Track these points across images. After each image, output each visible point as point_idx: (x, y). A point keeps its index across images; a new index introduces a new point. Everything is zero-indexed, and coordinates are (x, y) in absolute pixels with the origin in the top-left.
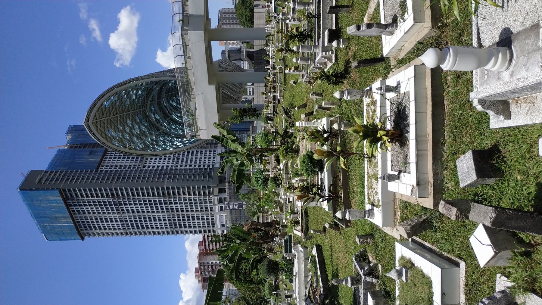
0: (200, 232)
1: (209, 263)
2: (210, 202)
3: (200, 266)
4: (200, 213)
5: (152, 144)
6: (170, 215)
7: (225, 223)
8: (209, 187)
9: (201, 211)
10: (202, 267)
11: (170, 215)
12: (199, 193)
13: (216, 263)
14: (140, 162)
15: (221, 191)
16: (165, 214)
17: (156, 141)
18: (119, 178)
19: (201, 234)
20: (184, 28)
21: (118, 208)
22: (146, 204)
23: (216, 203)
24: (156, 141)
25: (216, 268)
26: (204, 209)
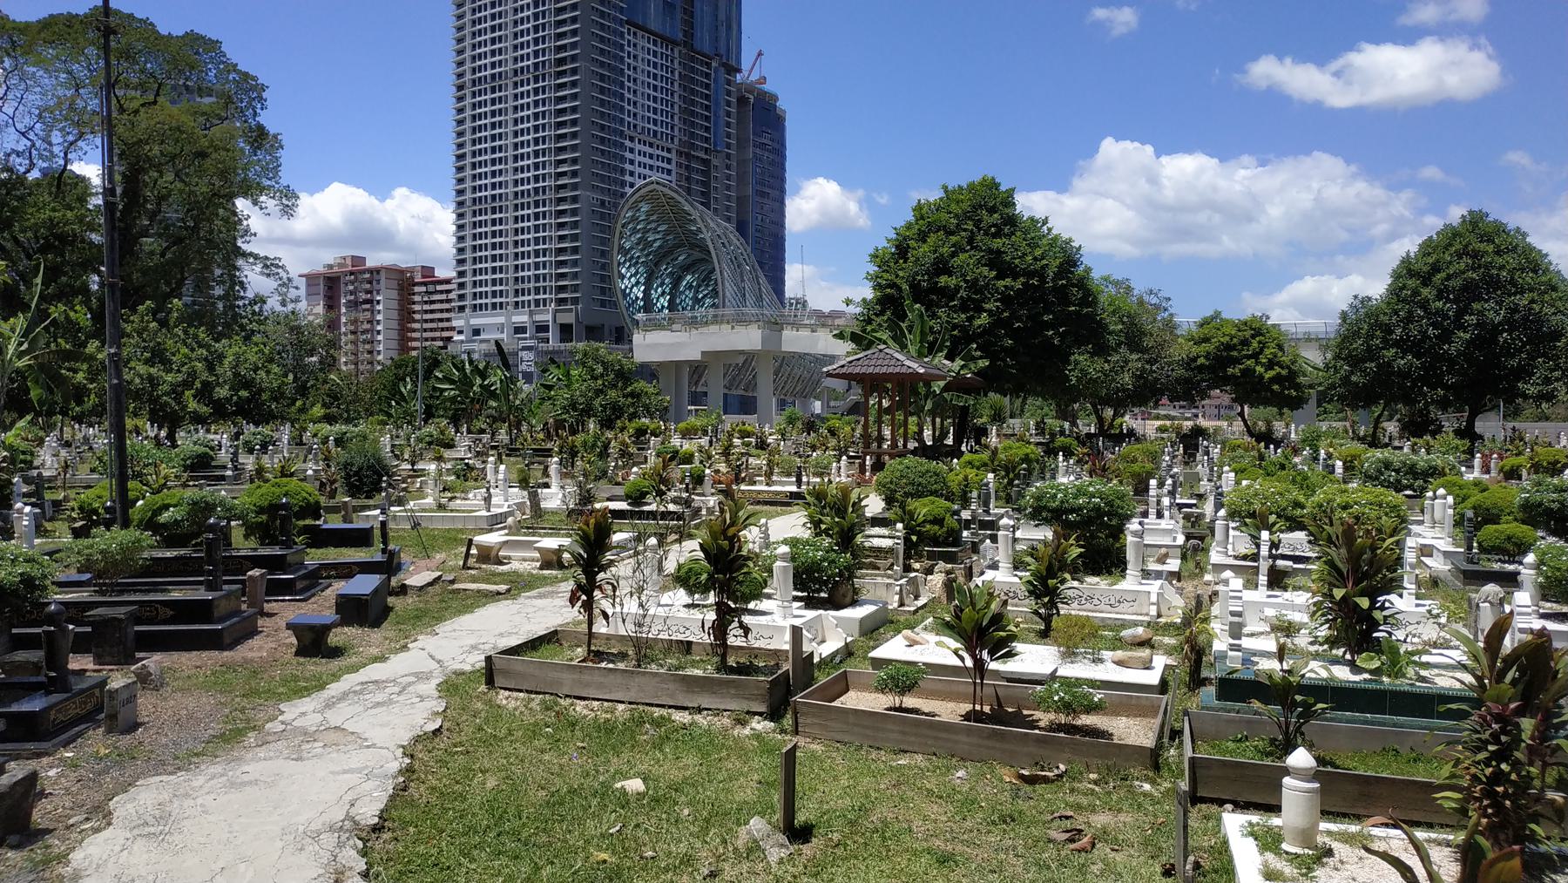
0: (461, 274)
1: (378, 293)
2: (537, 303)
3: (371, 271)
4: (511, 275)
5: (632, 258)
6: (507, 200)
7: (483, 337)
8: (575, 301)
9: (517, 279)
10: (367, 276)
11: (507, 200)
12: (562, 276)
13: (379, 312)
14: (643, 128)
15: (566, 332)
16: (511, 189)
17: (637, 263)
18: (602, 78)
19: (454, 274)
20: (89, 629)
21: (528, 71)
22: (536, 41)
23: (538, 318)
24: (637, 263)
25: (364, 310)
26: (520, 286)
